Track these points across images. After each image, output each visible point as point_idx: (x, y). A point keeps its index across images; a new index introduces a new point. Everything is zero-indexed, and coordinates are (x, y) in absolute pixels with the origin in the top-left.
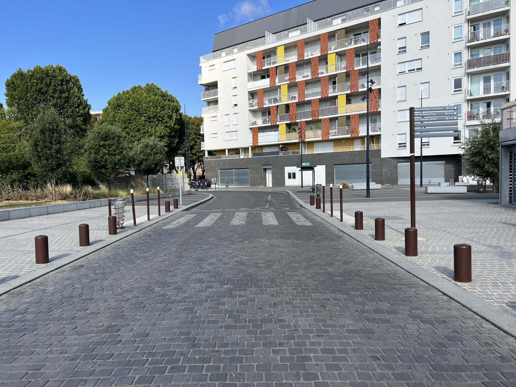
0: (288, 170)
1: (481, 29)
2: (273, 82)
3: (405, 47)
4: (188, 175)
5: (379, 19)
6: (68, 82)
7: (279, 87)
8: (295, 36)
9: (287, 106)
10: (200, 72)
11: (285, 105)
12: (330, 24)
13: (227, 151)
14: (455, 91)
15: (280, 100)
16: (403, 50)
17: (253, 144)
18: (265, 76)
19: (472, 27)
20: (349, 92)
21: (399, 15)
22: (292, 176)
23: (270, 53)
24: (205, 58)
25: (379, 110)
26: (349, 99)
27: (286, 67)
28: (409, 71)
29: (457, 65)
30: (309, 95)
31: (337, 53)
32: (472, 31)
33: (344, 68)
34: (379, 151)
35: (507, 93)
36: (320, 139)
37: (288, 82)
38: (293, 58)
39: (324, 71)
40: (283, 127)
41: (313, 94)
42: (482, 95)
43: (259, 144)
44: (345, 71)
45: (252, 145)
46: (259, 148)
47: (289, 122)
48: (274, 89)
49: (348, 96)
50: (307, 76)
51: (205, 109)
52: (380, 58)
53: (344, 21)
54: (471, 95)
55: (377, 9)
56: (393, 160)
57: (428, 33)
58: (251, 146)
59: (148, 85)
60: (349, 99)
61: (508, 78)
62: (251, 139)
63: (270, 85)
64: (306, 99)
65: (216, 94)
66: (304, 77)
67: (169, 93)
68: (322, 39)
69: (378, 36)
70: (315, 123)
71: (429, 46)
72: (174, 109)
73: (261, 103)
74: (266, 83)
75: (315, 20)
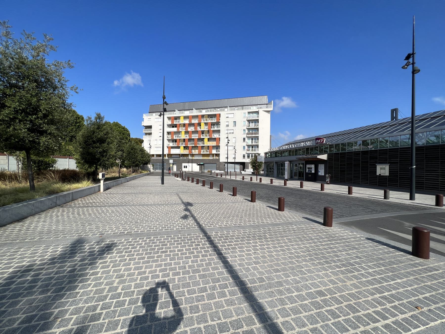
0: (184, 164)
1: (251, 123)
2: (178, 129)
6: (79, 118)
7: (181, 132)
8: (187, 113)
9: (184, 139)
10: (143, 121)
13: (155, 155)
22: (186, 167)
23: (178, 118)
26: (209, 140)
31: (205, 123)
34: (219, 159)
38: (187, 122)
40: (182, 148)
41: (195, 136)
48: (178, 133)
51: (144, 136)
60: (209, 140)
65: (151, 130)
68: (199, 117)
73: (172, 137)
74: (175, 129)
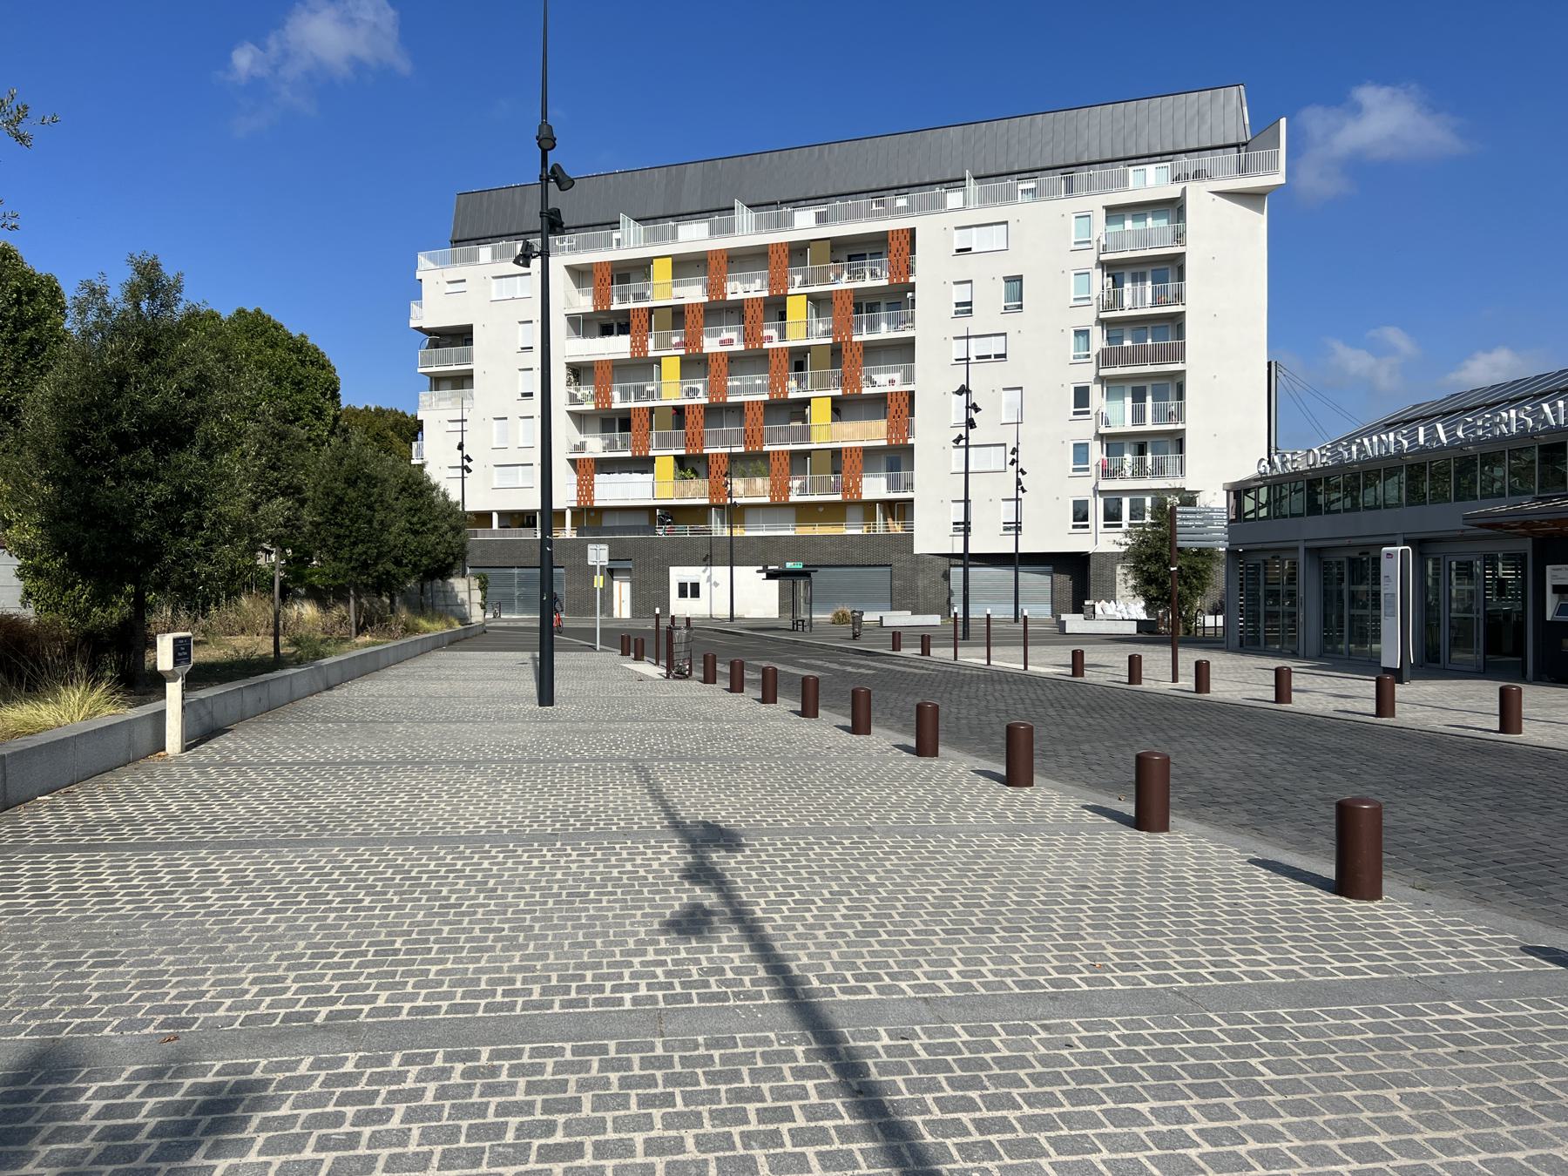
0: (678, 574)
1: (1128, 286)
3: (970, 303)
4: (482, 583)
5: (912, 231)
6: (32, 293)
7: (658, 361)
8: (694, 237)
9: (679, 411)
11: (675, 408)
12: (787, 223)
14: (1075, 413)
15: (659, 395)
16: (965, 308)
17: (579, 502)
18: (612, 326)
19: (1110, 279)
20: (839, 392)
21: (956, 228)
24: (431, 259)
25: (910, 441)
26: (840, 409)
27: (678, 315)
28: (978, 358)
29: (1079, 357)
30: (737, 391)
32: (1110, 286)
33: (826, 333)
34: (908, 539)
35: (1180, 426)
36: (767, 500)
37: (682, 352)
38: (693, 293)
39: (773, 333)
42: (1129, 427)
43: (596, 504)
44: (830, 341)
45: (575, 504)
46: (592, 514)
47: (682, 452)
48: (641, 367)
49: (834, 400)
50: (731, 342)
51: (426, 397)
52: (912, 320)
53: (821, 219)
54: (1107, 424)
55: (902, 202)
56: (941, 561)
57: (1019, 279)
58: (570, 508)
59: (258, 312)
60: (840, 409)
61: (1181, 395)
62: (574, 488)
63: (632, 353)
64: (730, 399)
65: (469, 358)
66: (723, 343)
67: (310, 342)
69: (910, 270)
70: (750, 462)
71: (1020, 307)
72: (327, 389)
74: (618, 347)
75: (750, 203)
